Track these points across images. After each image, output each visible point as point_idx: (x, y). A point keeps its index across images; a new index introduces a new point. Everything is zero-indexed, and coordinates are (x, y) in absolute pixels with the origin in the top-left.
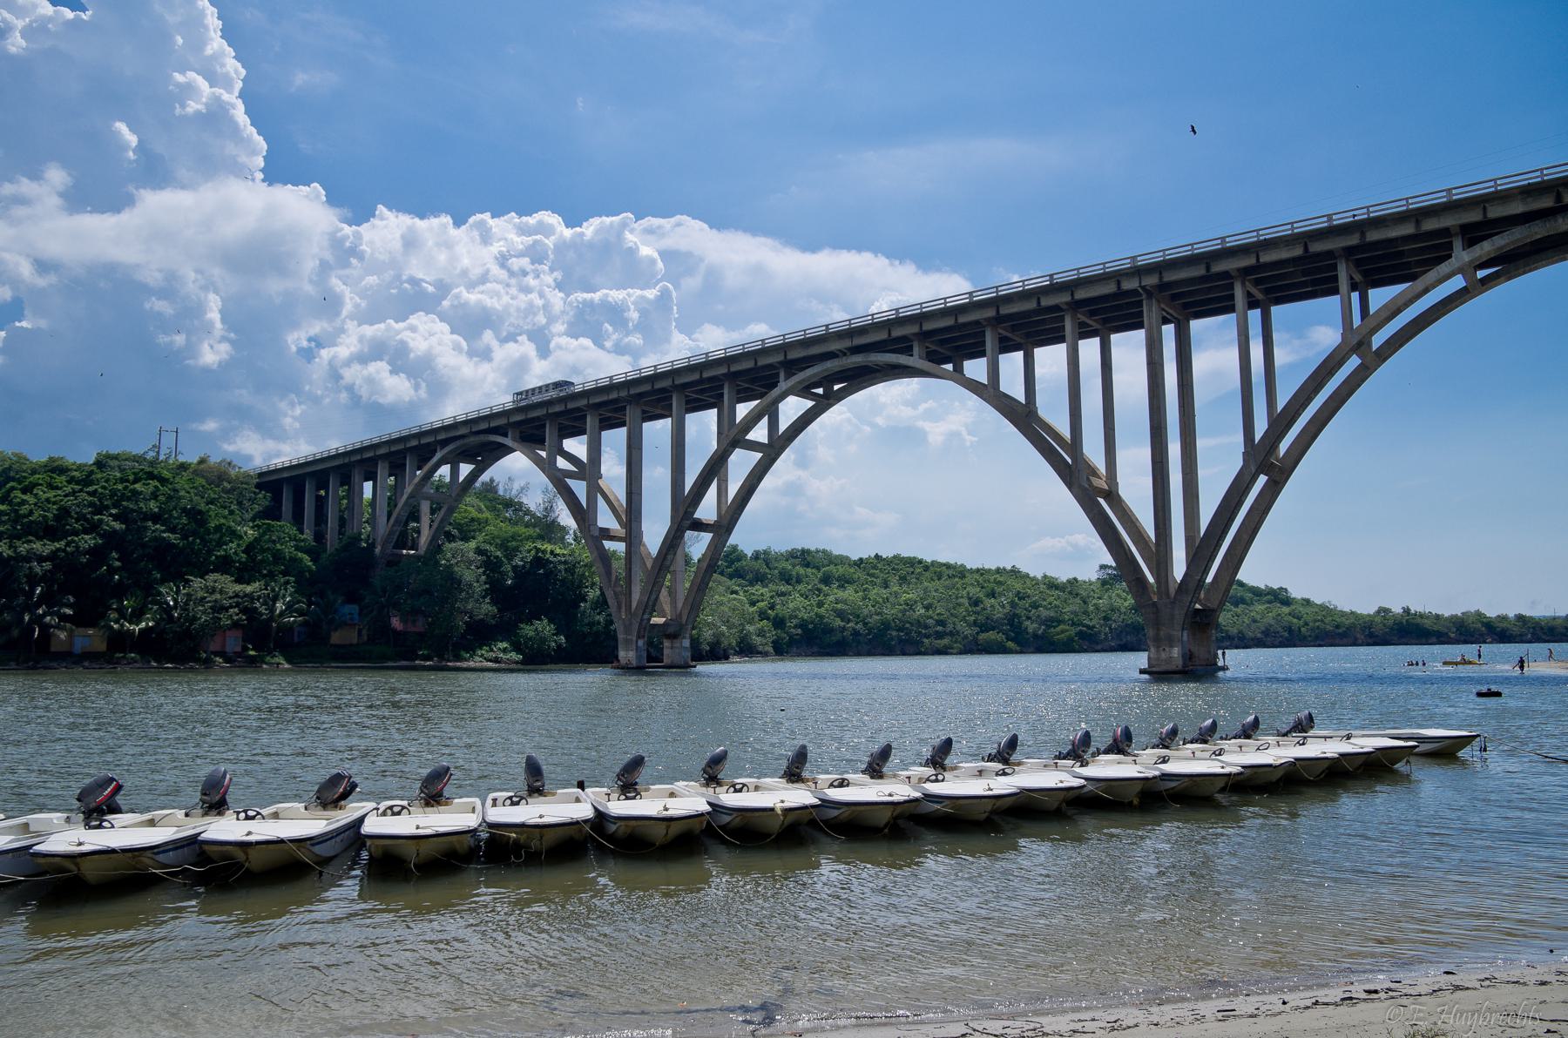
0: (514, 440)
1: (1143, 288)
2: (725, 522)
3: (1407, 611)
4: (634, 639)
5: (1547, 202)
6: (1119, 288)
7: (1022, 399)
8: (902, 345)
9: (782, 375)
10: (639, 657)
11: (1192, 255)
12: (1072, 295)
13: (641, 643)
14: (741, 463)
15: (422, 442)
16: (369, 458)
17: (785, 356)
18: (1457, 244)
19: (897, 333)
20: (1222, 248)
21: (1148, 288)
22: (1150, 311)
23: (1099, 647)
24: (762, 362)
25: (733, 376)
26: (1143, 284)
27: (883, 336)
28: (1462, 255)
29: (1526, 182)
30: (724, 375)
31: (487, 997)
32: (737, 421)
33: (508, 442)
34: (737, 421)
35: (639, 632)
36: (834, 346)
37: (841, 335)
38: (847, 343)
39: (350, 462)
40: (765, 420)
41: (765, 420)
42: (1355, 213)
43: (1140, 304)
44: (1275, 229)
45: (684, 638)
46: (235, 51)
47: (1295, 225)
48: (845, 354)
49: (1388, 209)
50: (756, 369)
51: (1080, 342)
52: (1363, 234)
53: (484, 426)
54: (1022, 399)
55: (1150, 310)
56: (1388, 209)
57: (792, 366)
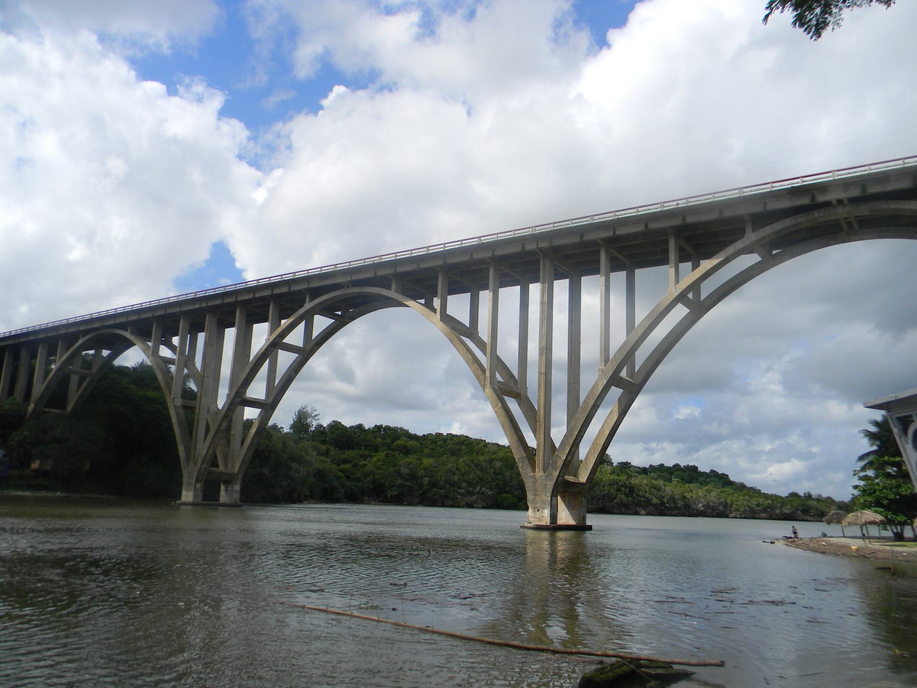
0: (132, 333)
1: (540, 249)
2: (270, 401)
4: (194, 481)
5: (806, 201)
6: (523, 248)
7: (467, 323)
8: (385, 282)
9: (307, 300)
10: (195, 496)
11: (771, 192)
14: (285, 359)
15: (225, 302)
17: (290, 289)
18: (749, 229)
20: (687, 206)
21: (543, 249)
22: (545, 268)
23: (637, 469)
24: (295, 288)
25: (277, 298)
26: (539, 246)
28: (751, 237)
29: (790, 186)
32: (304, 321)
33: (127, 335)
34: (304, 321)
36: (340, 280)
37: (344, 272)
39: (208, 307)
41: (303, 324)
42: (678, 202)
43: (538, 262)
45: (236, 484)
46: (163, 82)
47: (446, 245)
48: (348, 286)
49: (605, 218)
51: (449, 297)
53: (111, 322)
54: (467, 323)
55: (544, 265)
57: (315, 293)
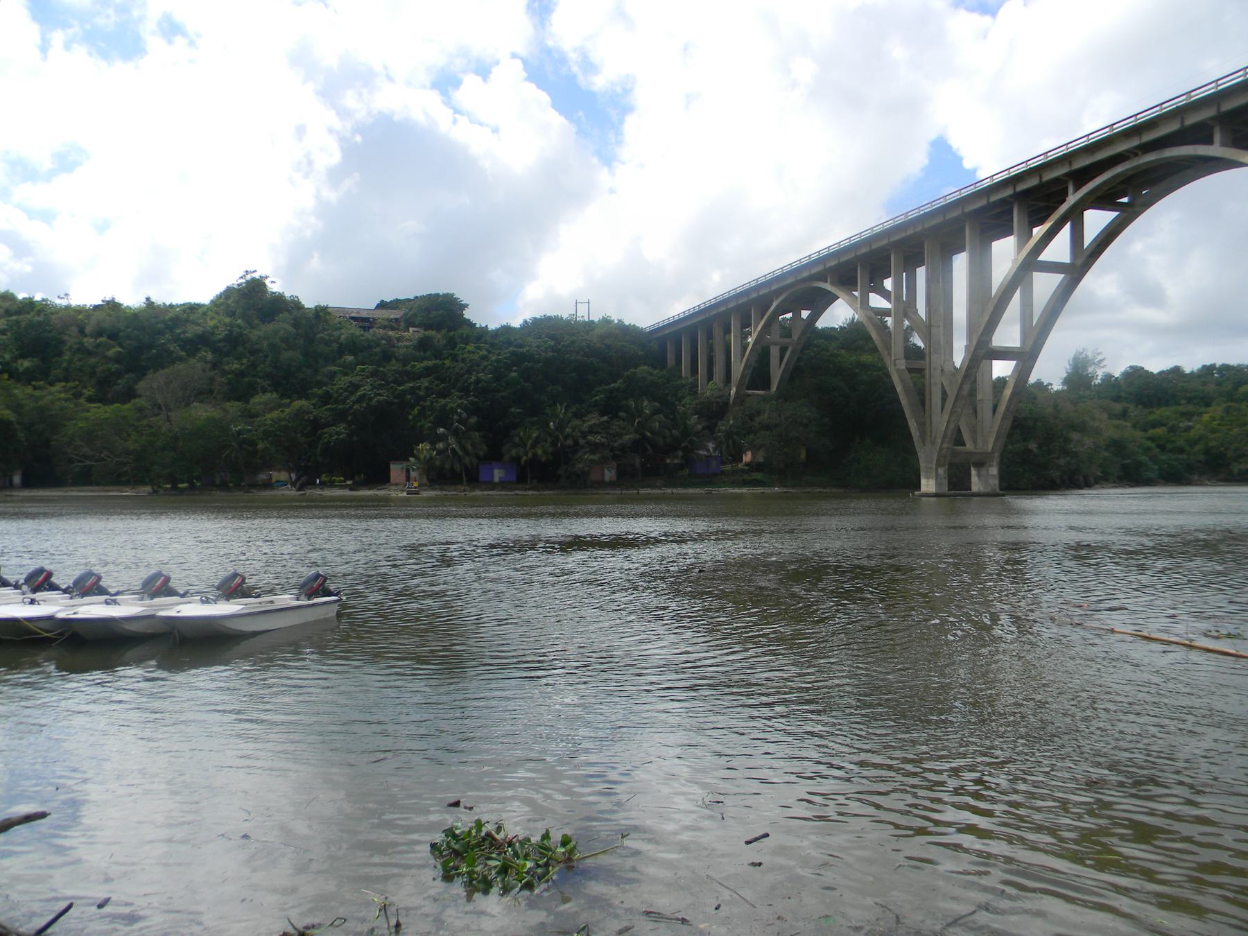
3: (150, 303)
8: (1201, 134)
9: (1071, 189)
10: (938, 485)
12: (963, 209)
13: (941, 471)
15: (947, 218)
16: (789, 284)
19: (1191, 120)
27: (1173, 127)
30: (1011, 196)
31: (1067, 775)
32: (1085, 246)
33: (827, 286)
34: (1085, 246)
35: (938, 460)
38: (1134, 142)
40: (1042, 257)
44: (951, 196)
49: (1224, 83)
50: (1041, 186)
52: (871, 246)
56: (1224, 83)
